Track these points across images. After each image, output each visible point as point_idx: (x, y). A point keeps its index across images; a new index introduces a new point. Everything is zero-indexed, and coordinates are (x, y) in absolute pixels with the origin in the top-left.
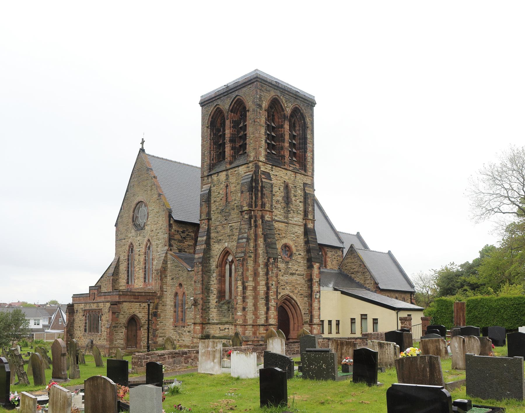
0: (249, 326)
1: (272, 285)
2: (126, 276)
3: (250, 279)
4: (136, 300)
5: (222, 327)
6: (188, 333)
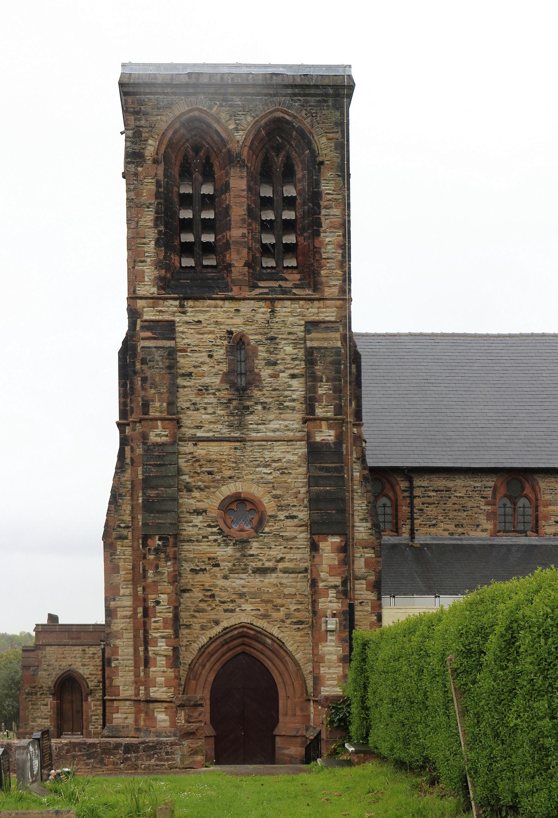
0: (122, 703)
1: (158, 603)
3: (122, 591)
4: (74, 641)
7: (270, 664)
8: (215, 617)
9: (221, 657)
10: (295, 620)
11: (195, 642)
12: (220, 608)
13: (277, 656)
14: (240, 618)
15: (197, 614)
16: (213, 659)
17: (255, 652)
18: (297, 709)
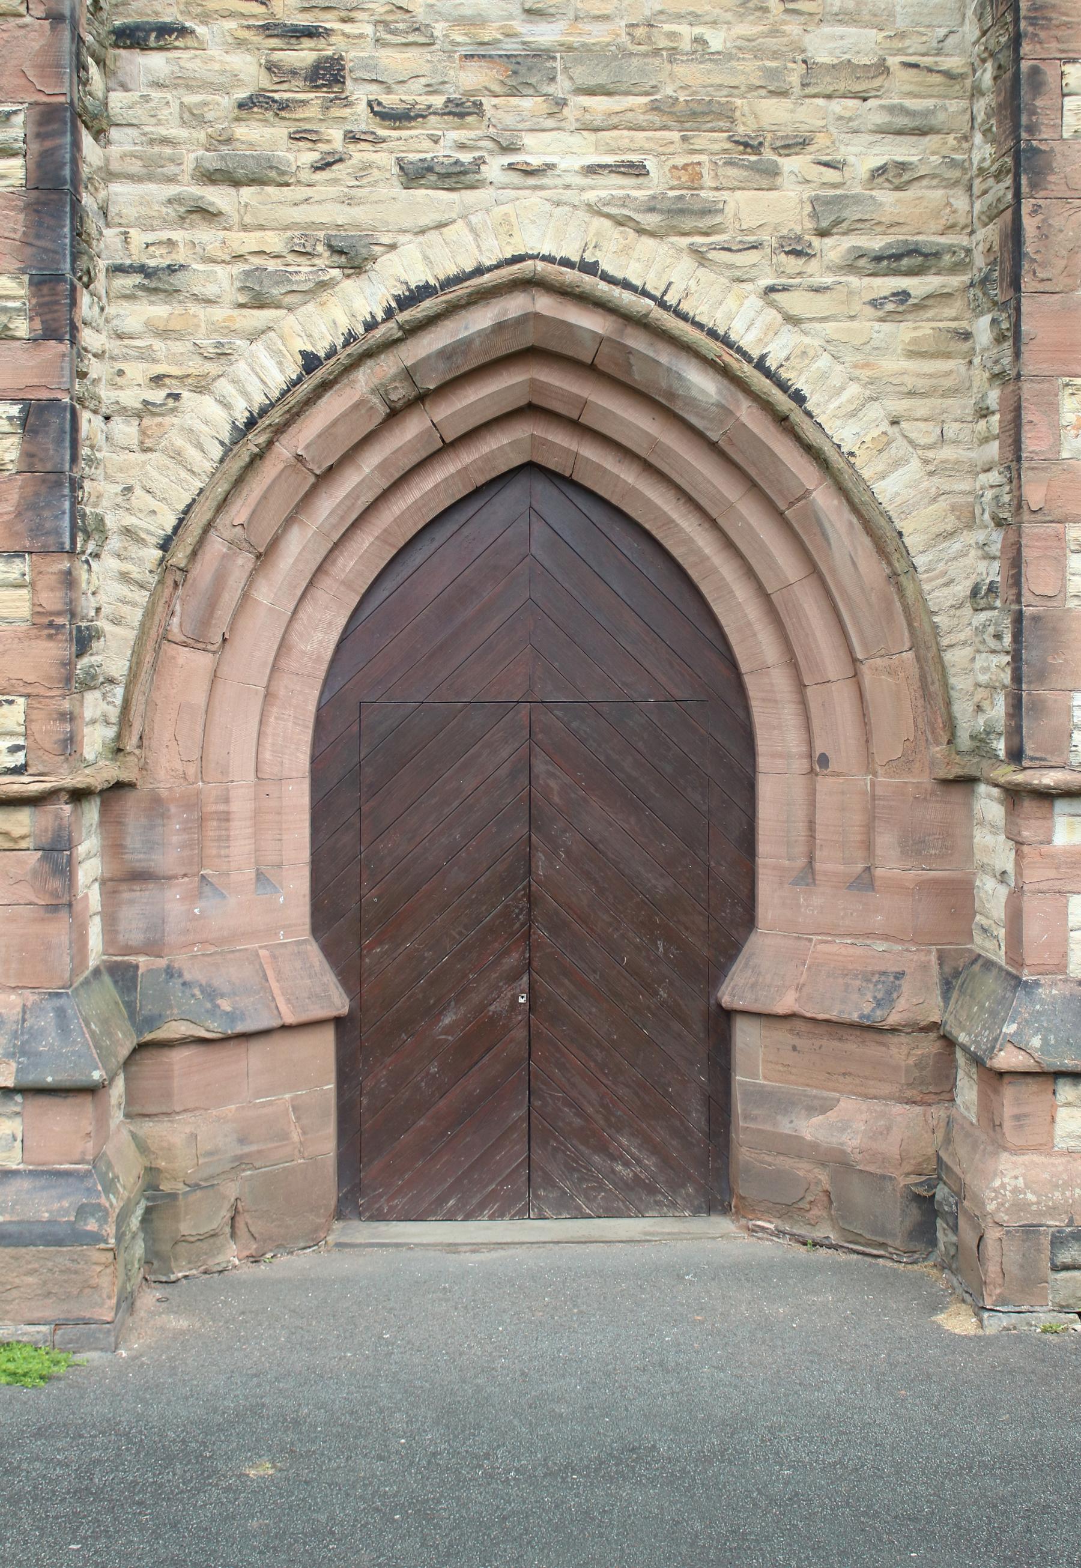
7: (704, 541)
8: (341, 215)
9: (385, 496)
10: (876, 243)
11: (201, 386)
12: (384, 159)
13: (753, 486)
14: (506, 228)
15: (218, 197)
16: (329, 505)
17: (608, 462)
18: (886, 840)
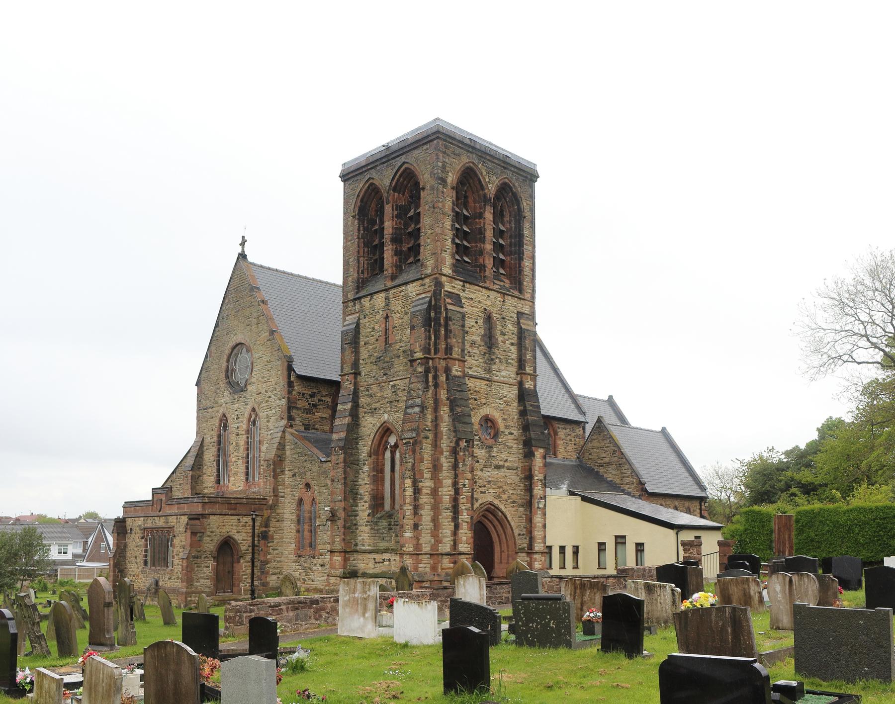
0: (424, 556)
1: (464, 485)
2: (215, 470)
3: (426, 476)
4: (232, 512)
5: (379, 557)
6: (320, 568)
